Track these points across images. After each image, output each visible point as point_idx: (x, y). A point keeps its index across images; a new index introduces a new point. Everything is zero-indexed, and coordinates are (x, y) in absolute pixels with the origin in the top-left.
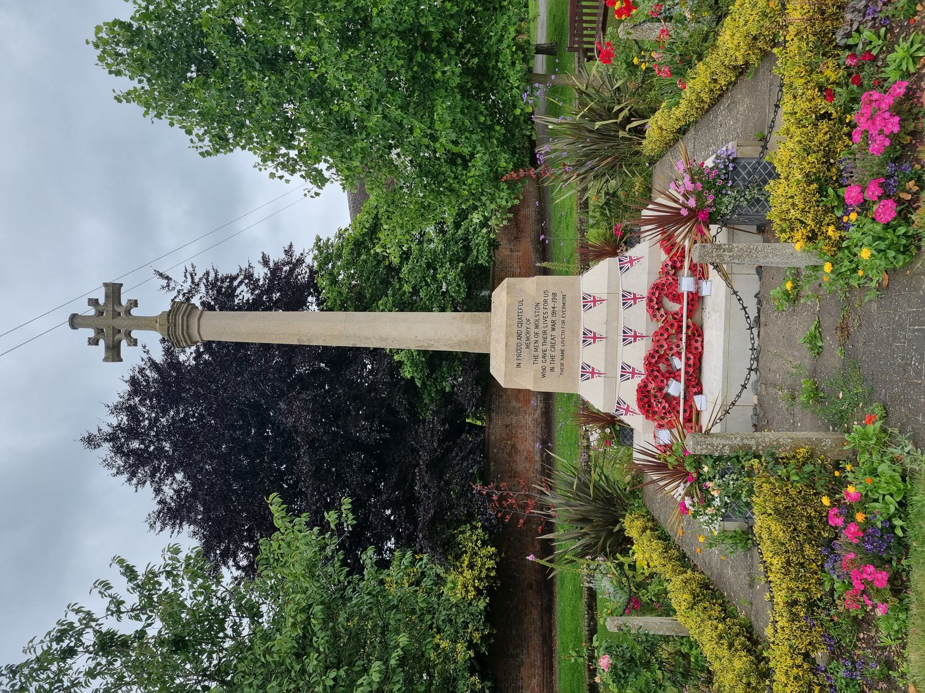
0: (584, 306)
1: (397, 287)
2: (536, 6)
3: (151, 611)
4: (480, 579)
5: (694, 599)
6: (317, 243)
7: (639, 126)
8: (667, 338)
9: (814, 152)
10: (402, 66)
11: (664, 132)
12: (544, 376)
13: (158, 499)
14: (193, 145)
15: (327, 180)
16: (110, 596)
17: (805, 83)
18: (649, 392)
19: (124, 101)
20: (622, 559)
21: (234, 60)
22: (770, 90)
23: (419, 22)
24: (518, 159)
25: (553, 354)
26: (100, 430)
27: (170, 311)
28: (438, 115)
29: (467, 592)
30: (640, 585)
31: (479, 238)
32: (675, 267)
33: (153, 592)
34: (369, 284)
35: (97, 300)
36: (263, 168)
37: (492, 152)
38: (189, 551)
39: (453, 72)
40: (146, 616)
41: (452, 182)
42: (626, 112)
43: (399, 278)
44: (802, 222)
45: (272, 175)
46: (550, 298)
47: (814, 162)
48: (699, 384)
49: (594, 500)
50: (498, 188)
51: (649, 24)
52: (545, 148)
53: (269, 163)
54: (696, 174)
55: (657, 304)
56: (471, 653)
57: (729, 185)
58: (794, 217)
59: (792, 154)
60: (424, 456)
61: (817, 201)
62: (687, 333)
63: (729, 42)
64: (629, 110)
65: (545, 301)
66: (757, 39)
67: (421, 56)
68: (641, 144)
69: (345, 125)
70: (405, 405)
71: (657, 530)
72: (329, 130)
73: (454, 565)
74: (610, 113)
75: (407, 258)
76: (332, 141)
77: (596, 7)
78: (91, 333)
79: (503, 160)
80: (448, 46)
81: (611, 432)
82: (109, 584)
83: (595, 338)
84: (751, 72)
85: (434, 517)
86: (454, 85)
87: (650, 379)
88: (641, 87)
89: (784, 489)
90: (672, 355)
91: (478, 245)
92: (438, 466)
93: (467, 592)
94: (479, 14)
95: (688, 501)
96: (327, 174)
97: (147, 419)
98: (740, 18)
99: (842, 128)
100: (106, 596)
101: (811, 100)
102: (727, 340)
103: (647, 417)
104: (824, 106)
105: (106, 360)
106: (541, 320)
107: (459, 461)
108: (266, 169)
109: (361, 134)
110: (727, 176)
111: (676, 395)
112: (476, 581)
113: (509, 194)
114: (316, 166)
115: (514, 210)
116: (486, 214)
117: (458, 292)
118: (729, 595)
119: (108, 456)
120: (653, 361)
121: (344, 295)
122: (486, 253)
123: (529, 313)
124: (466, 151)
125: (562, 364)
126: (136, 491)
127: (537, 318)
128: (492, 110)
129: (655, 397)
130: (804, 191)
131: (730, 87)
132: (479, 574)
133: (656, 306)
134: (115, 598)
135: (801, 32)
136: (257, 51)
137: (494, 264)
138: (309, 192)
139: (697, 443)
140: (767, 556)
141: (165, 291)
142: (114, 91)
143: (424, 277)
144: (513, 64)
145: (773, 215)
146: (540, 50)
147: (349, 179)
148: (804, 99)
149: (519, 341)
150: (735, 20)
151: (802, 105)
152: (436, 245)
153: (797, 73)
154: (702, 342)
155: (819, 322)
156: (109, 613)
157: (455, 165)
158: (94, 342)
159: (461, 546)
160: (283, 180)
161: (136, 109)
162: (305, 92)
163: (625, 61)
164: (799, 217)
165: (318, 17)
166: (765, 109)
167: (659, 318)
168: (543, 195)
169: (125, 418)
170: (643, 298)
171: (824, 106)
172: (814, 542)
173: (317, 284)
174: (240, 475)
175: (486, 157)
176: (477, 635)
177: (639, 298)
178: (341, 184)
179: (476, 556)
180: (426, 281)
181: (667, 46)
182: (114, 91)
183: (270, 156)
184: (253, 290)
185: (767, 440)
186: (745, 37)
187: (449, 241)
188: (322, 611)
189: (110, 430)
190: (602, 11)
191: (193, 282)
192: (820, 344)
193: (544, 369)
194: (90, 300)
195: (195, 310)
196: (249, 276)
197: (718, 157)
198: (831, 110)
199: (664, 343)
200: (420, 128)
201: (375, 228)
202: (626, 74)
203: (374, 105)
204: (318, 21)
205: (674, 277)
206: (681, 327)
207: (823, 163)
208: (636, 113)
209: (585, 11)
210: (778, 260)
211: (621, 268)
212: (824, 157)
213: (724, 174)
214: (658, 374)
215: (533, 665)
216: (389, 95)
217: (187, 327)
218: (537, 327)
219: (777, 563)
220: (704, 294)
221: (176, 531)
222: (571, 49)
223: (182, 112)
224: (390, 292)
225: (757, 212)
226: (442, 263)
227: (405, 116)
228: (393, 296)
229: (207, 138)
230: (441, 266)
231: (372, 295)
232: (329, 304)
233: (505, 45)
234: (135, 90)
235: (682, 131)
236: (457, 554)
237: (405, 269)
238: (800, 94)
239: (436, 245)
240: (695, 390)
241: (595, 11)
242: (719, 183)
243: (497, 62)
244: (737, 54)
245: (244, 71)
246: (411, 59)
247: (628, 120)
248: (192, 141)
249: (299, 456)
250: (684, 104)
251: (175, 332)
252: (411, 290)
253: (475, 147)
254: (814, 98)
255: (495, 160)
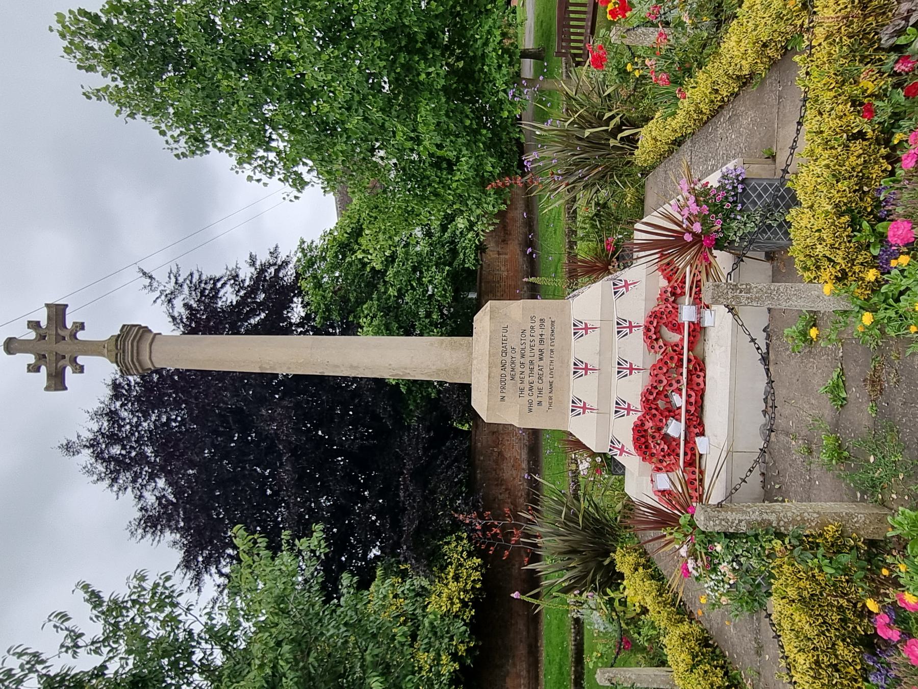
0: (575, 333)
1: (383, 290)
2: (524, 12)
3: (114, 642)
4: (466, 591)
5: (693, 660)
6: (301, 245)
7: (631, 135)
8: (667, 372)
9: (845, 179)
10: (384, 67)
11: (659, 143)
12: (530, 411)
13: (140, 506)
14: (168, 146)
15: (307, 183)
16: (67, 629)
17: (835, 97)
18: (646, 431)
19: (94, 98)
20: (612, 595)
21: (210, 59)
22: (779, 103)
23: (402, 23)
24: (505, 164)
25: (541, 386)
26: (79, 436)
27: (119, 335)
28: (421, 117)
29: (452, 604)
30: (634, 621)
31: (467, 241)
32: (676, 294)
33: (120, 619)
34: (353, 288)
35: (38, 323)
36: (240, 171)
37: (478, 156)
38: (158, 578)
39: (438, 74)
40: (109, 648)
41: (436, 186)
42: (617, 119)
43: (385, 282)
44: (830, 260)
45: (250, 178)
46: (538, 323)
47: (844, 191)
48: (701, 424)
49: (584, 529)
50: (485, 193)
51: (643, 29)
52: (534, 155)
53: (246, 166)
54: (702, 196)
55: (655, 333)
56: (457, 666)
57: (738, 209)
58: (821, 254)
59: (819, 180)
60: (409, 465)
61: (848, 236)
62: (688, 368)
63: (735, 49)
64: (621, 118)
65: (532, 328)
66: (767, 46)
67: (404, 57)
68: (633, 154)
69: (327, 128)
70: (390, 411)
71: (650, 567)
72: (308, 132)
73: (439, 577)
74: (600, 120)
75: (393, 261)
76: (311, 144)
77: (584, 13)
78: (31, 359)
79: (490, 165)
80: (433, 48)
81: (602, 461)
82: (66, 615)
83: (586, 369)
84: (757, 83)
85: (418, 528)
86: (439, 87)
87: (647, 417)
88: (633, 95)
89: (810, 573)
90: (673, 391)
91: (465, 248)
92: (422, 475)
93: (452, 604)
94: (464, 17)
95: (691, 564)
96: (307, 177)
97: (128, 423)
98: (748, 22)
99: (879, 149)
100: (62, 629)
101: (841, 117)
102: (734, 379)
103: (644, 459)
104: (859, 123)
105: (47, 389)
106: (528, 349)
107: (443, 469)
108: (243, 172)
109: (341, 137)
110: (735, 198)
111: (676, 436)
112: (462, 593)
113: (496, 199)
114: (295, 169)
115: (501, 215)
116: (472, 219)
117: (444, 296)
118: (731, 655)
119: (88, 463)
120: (651, 397)
121: (328, 299)
122: (473, 256)
123: (514, 341)
124: (452, 155)
125: (551, 398)
126: (118, 498)
127: (523, 347)
128: (479, 113)
129: (653, 437)
130: (833, 224)
131: (732, 98)
132: (465, 586)
133: (654, 337)
134: (73, 631)
135: (832, 34)
136: (233, 51)
137: (481, 268)
138: (288, 195)
139: (709, 519)
140: (790, 649)
141: (147, 291)
142: (82, 87)
143: (410, 281)
144: (500, 67)
145: (796, 251)
146: (525, 54)
147: (331, 182)
148: (833, 116)
149: (503, 372)
150: (742, 25)
151: (830, 123)
152: (422, 247)
153: (825, 84)
154: (705, 377)
155: (842, 370)
156: (64, 649)
157: (441, 169)
158: (34, 369)
159: (446, 557)
160: (261, 183)
161: (107, 108)
162: (283, 93)
163: (616, 67)
164: (827, 255)
165: (297, 15)
166: (773, 123)
167: (657, 349)
168: (530, 205)
169: (106, 424)
170: (640, 326)
171: (859, 123)
172: (848, 640)
173: (300, 287)
174: (222, 483)
175: (472, 161)
176: (462, 648)
177: (635, 327)
178: (322, 188)
179: (462, 567)
180: (412, 285)
181: (663, 52)
182: (82, 87)
183: (246, 158)
184: (238, 291)
185: (789, 514)
186: (754, 43)
187: (436, 244)
188: (291, 651)
189: (91, 436)
190: (591, 16)
191: (176, 283)
192: (843, 395)
193: (531, 404)
194: (29, 322)
195: (148, 334)
196: (235, 277)
197: (724, 177)
198: (868, 129)
199: (663, 378)
200: (402, 132)
201: (357, 233)
202: (617, 81)
203: (355, 107)
204: (297, 19)
205: (674, 305)
206: (681, 360)
207: (855, 191)
208: (628, 121)
209: (572, 16)
210: (803, 304)
211: (615, 293)
212: (856, 185)
213: (733, 196)
214: (656, 412)
215: (519, 676)
216: (370, 97)
217: (138, 353)
218: (523, 356)
219: (803, 661)
220: (706, 325)
221: (157, 538)
222: (559, 54)
223: (157, 112)
224: (375, 296)
225: (769, 239)
226: (428, 267)
227: (387, 119)
228: (378, 300)
229: (183, 140)
230: (427, 270)
231: (357, 298)
232: (313, 308)
233: (491, 49)
234: (107, 87)
235: (678, 142)
236: (442, 566)
237: (390, 273)
238: (828, 110)
239: (422, 247)
240: (697, 430)
241: (583, 16)
242: (727, 206)
243: (483, 65)
244: (744, 62)
245: (221, 71)
246: (394, 62)
247: (619, 129)
248: (167, 142)
249: (281, 464)
250: (681, 114)
251: (124, 359)
252: (396, 294)
253: (461, 150)
254: (845, 115)
255: (481, 164)
